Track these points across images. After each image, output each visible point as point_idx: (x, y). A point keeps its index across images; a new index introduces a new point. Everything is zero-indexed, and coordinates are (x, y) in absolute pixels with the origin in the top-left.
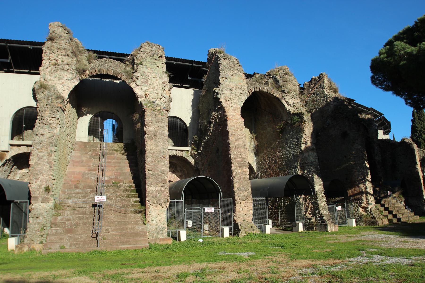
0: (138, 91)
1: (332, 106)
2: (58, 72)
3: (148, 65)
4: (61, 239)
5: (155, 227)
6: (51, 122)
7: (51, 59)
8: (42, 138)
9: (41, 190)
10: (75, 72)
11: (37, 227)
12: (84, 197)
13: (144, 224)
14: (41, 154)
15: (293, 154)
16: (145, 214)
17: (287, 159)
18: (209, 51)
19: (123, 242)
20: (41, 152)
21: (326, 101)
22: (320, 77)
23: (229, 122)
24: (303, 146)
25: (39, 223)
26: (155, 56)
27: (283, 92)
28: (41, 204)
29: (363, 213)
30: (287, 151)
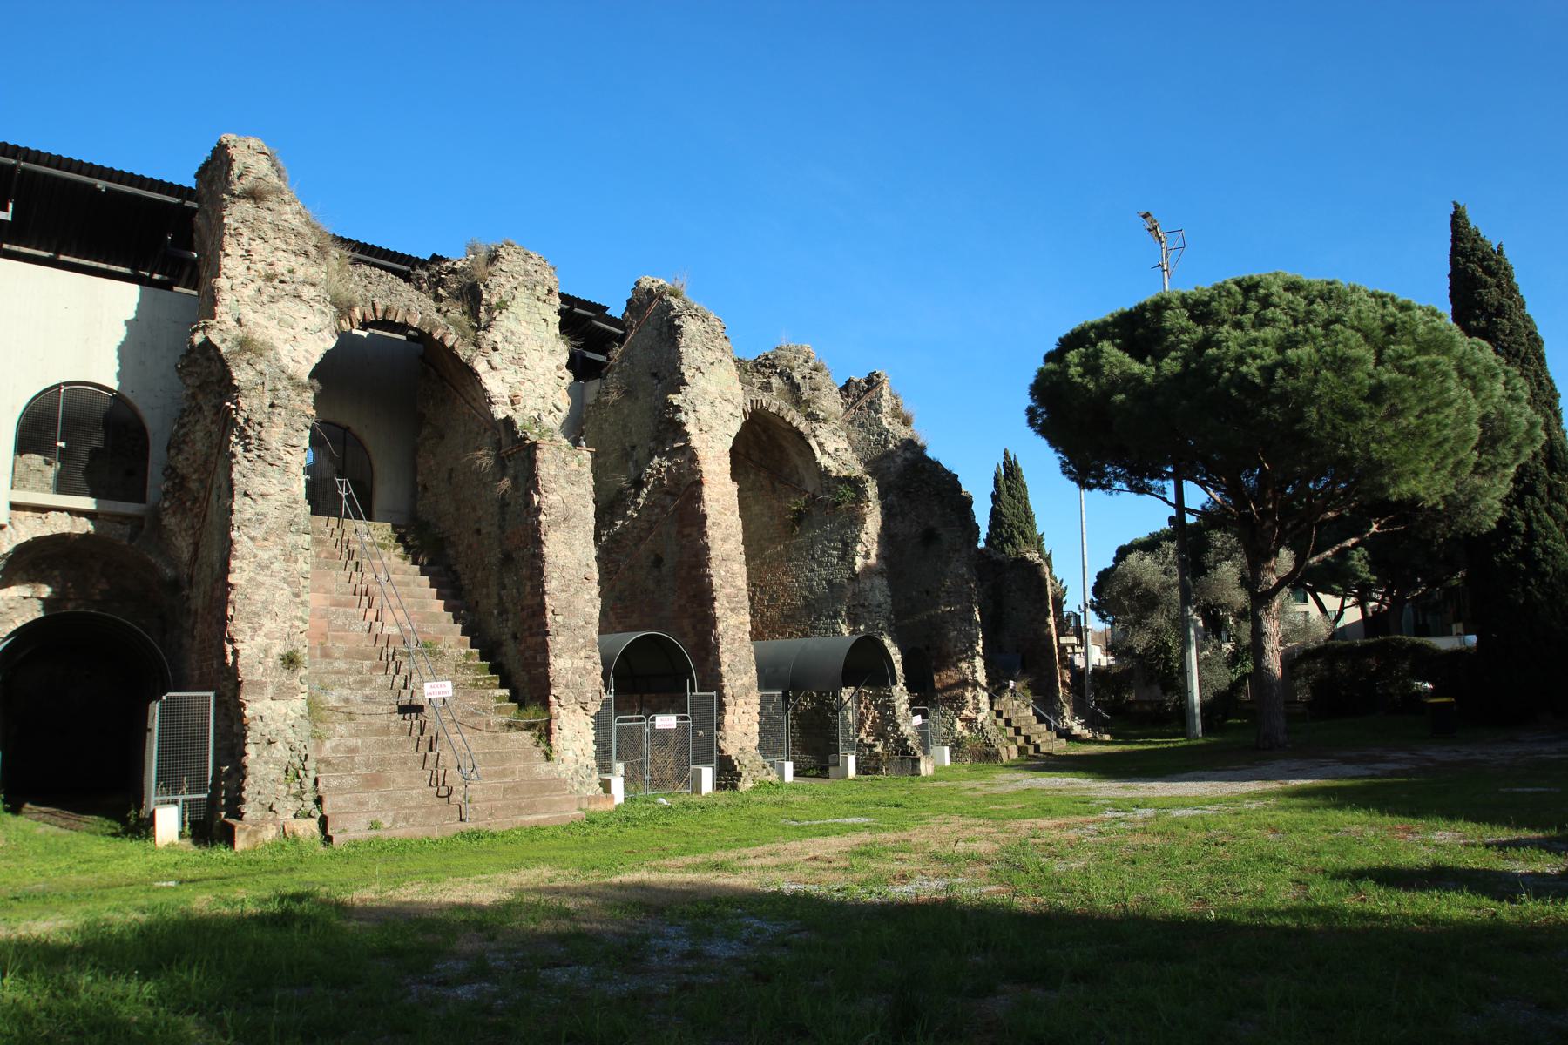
0: (493, 384)
1: (899, 460)
2: (281, 304)
3: (522, 313)
4: (361, 804)
5: (573, 766)
6: (288, 458)
7: (255, 257)
8: (262, 505)
9: (270, 663)
10: (331, 310)
11: (276, 773)
12: (363, 683)
13: (548, 758)
14: (264, 556)
15: (829, 582)
16: (549, 732)
17: (811, 592)
18: (637, 283)
19: (520, 808)
20: (262, 548)
21: (884, 447)
22: (872, 382)
23: (706, 491)
24: (859, 563)
25: (277, 762)
26: (539, 288)
27: (812, 417)
28: (271, 703)
29: (966, 733)
30: (812, 570)
